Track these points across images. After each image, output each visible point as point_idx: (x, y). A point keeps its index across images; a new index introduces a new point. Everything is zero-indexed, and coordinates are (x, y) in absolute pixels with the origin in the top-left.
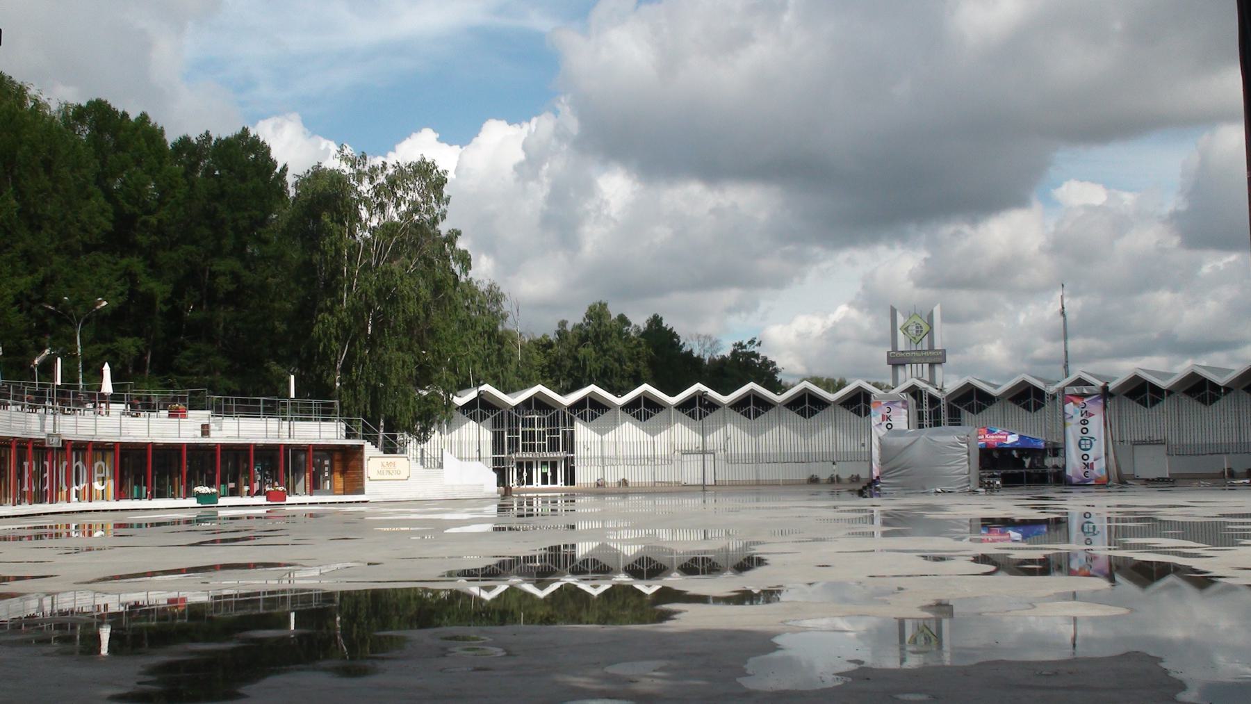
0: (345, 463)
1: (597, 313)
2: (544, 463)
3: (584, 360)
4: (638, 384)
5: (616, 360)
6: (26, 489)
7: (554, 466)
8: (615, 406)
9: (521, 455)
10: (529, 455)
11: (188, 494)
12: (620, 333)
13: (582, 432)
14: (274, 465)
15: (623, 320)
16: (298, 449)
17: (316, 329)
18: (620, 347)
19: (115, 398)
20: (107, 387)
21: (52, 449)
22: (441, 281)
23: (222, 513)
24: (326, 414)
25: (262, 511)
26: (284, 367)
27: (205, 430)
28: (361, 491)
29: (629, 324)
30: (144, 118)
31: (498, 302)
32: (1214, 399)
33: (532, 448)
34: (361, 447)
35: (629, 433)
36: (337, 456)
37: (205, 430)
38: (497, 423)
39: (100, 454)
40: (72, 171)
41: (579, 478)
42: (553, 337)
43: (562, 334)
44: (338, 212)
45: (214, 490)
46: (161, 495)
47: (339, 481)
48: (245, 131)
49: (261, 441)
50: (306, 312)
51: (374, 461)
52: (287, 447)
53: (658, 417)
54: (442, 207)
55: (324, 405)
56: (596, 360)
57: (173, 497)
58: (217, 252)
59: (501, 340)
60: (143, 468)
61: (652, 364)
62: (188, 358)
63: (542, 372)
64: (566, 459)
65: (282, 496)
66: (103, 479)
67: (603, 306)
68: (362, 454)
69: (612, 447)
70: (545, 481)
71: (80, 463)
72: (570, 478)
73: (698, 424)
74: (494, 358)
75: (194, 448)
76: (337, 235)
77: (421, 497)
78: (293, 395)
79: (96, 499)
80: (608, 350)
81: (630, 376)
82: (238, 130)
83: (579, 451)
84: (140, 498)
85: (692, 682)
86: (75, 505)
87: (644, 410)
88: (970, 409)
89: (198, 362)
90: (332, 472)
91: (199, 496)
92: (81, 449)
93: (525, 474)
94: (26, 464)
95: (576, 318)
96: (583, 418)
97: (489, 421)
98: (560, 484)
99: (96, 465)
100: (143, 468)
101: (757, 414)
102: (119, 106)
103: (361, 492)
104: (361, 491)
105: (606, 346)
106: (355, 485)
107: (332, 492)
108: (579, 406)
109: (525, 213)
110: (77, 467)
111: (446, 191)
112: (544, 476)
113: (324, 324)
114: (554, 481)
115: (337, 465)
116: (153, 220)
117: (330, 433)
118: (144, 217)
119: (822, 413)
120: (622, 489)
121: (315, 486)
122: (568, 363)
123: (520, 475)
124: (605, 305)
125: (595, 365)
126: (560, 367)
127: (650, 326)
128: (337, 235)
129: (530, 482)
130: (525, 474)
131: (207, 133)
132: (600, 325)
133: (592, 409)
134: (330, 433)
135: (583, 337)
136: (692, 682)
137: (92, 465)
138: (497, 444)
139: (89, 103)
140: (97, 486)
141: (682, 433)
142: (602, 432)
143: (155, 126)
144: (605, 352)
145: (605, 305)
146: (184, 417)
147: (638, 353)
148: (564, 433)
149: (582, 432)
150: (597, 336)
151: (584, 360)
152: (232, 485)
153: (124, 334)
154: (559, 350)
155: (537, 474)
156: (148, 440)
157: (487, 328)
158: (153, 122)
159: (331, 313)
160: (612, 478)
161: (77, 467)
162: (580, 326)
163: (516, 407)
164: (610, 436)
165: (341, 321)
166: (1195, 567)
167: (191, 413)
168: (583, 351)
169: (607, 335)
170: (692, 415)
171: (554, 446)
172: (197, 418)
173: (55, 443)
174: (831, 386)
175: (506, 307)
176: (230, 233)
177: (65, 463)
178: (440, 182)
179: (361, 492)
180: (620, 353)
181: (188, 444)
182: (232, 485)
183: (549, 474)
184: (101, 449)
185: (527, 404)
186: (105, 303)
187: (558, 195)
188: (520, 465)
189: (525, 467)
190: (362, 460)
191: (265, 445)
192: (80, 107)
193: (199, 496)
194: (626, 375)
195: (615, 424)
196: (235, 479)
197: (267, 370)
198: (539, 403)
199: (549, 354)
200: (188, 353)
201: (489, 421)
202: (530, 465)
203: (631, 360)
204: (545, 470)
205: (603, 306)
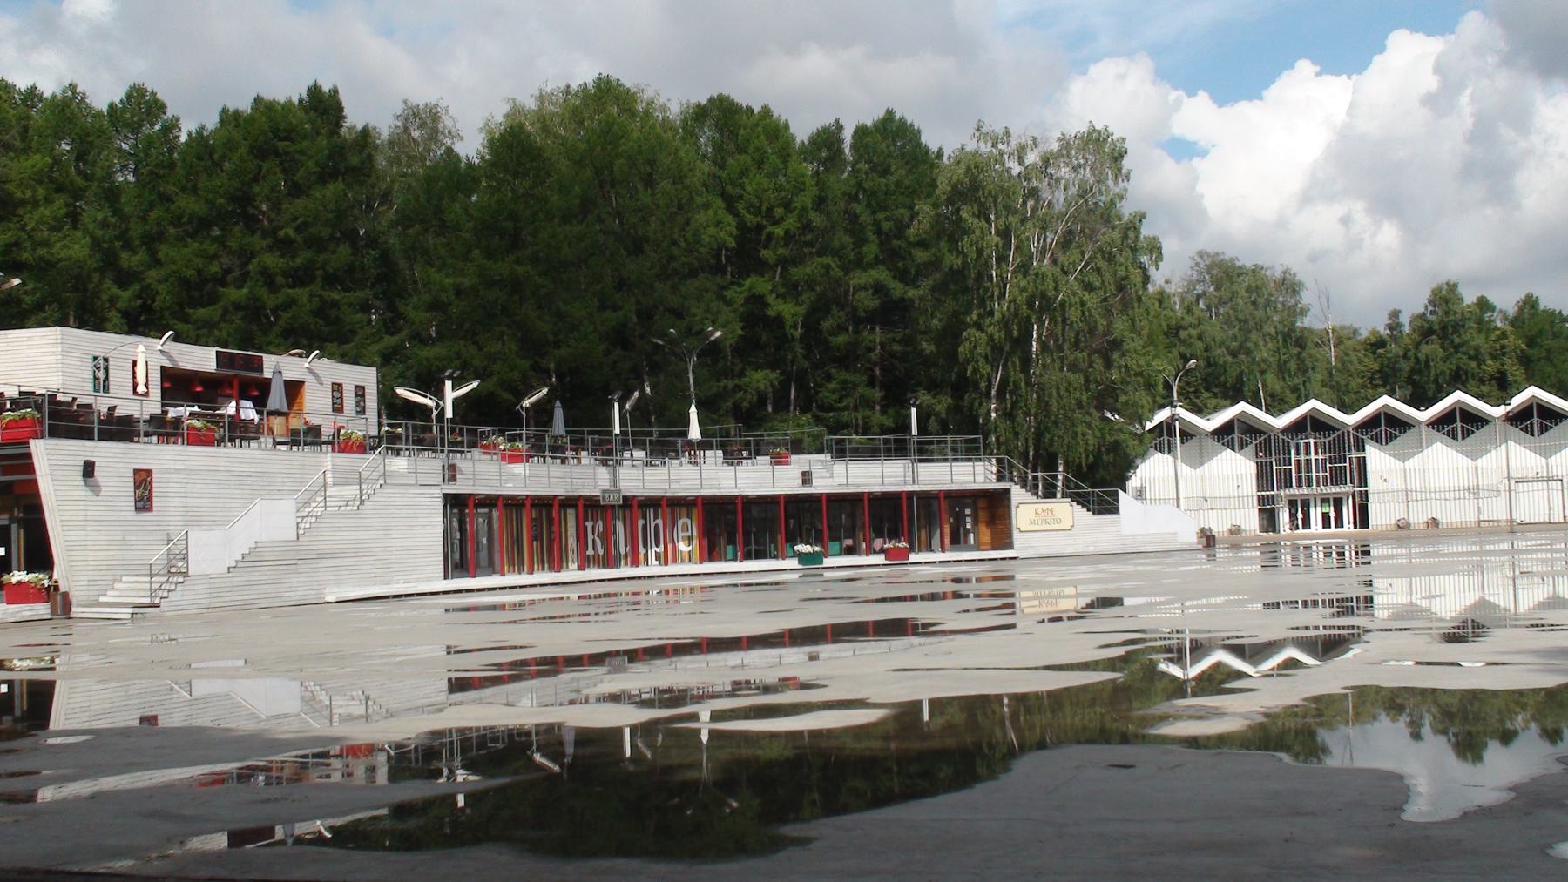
0: (991, 510)
1: (1445, 297)
2: (1325, 501)
3: (1427, 362)
4: (1235, 402)
5: (1471, 358)
6: (590, 552)
7: (1338, 504)
9: (1295, 491)
10: (1304, 490)
11: (871, 551)
12: (1480, 321)
13: (1377, 458)
14: (890, 520)
15: (1483, 304)
16: (927, 500)
17: (961, 349)
18: (1479, 340)
19: (704, 445)
20: (695, 433)
22: (1123, 279)
23: (828, 574)
24: (971, 452)
25: (795, 576)
26: (934, 396)
27: (807, 478)
28: (1009, 545)
29: (1492, 308)
30: (766, 111)
31: (1295, 292)
34: (1007, 491)
35: (1441, 461)
36: (981, 503)
37: (807, 478)
39: (684, 510)
40: (674, 183)
41: (1373, 518)
42: (1384, 332)
43: (1394, 326)
44: (981, 205)
45: (817, 549)
46: (760, 555)
47: (986, 534)
48: (890, 113)
49: (877, 489)
50: (952, 334)
51: (1026, 510)
52: (910, 494)
53: (1481, 434)
54: (1121, 185)
55: (967, 441)
56: (1444, 360)
57: (776, 557)
58: (860, 264)
59: (1301, 343)
60: (734, 526)
61: (1525, 360)
62: (834, 392)
63: (1372, 379)
65: (904, 554)
66: (690, 539)
67: (1453, 287)
68: (1009, 500)
69: (1417, 477)
70: (1326, 524)
71: (660, 522)
72: (1362, 518)
73: (1537, 441)
74: (1293, 365)
75: (793, 501)
76: (978, 232)
77: (1091, 550)
78: (915, 431)
79: (681, 561)
80: (1462, 345)
81: (1492, 378)
82: (881, 114)
83: (1374, 484)
84: (735, 559)
86: (654, 568)
87: (1460, 425)
89: (848, 395)
90: (976, 522)
91: (802, 557)
92: (649, 506)
93: (1300, 515)
94: (589, 524)
95: (1414, 303)
96: (1377, 439)
97: (1251, 449)
98: (1348, 526)
99: (680, 523)
100: (734, 526)
102: (741, 99)
103: (1010, 546)
104: (1009, 545)
105: (1457, 340)
106: (1003, 539)
107: (977, 547)
108: (1371, 424)
109: (1265, 174)
110: (657, 527)
111: (1126, 163)
112: (1326, 517)
113: (974, 342)
114: (1339, 523)
115: (982, 515)
116: (779, 231)
117: (975, 475)
118: (769, 229)
120: (1432, 531)
121: (957, 540)
122: (1405, 366)
123: (1293, 516)
124: (1455, 285)
125: (1442, 367)
126: (1395, 371)
127: (1521, 309)
128: (978, 232)
129: (1306, 524)
130: (1300, 515)
131: (837, 121)
132: (1447, 313)
133: (1388, 428)
134: (975, 475)
135: (1425, 330)
137: (674, 524)
138: (1264, 476)
139: (711, 100)
140: (683, 547)
141: (1519, 455)
142: (1403, 458)
143: (778, 120)
144: (1457, 348)
145: (1455, 285)
146: (787, 463)
147: (1503, 347)
149: (1377, 458)
150: (1444, 328)
151: (1427, 362)
152: (849, 542)
153: (758, 367)
154: (1393, 349)
155: (1316, 514)
156: (735, 492)
157: (1280, 328)
158: (776, 115)
159: (979, 327)
160: (1418, 518)
161: (657, 527)
162: (1422, 316)
163: (1286, 430)
164: (1414, 462)
165: (991, 338)
166: (754, 676)
167: (794, 458)
168: (1425, 349)
169: (1457, 327)
170: (1529, 431)
171: (1337, 477)
172: (799, 462)
173: (614, 499)
175: (1307, 297)
176: (873, 237)
177: (640, 523)
178: (1118, 156)
179: (1010, 546)
180: (1477, 349)
181: (829, 495)
182: (849, 542)
183: (1332, 515)
184: (675, 506)
185: (1298, 427)
186: (718, 334)
187: (1482, 133)
188: (1292, 504)
189: (1300, 507)
190: (1009, 507)
191: (884, 494)
192: (699, 105)
193: (802, 557)
194: (1487, 377)
195: (1420, 448)
196: (852, 535)
198: (1315, 423)
199: (1380, 356)
200: (833, 385)
201: (1251, 449)
202: (1306, 505)
203: (1494, 358)
204: (1326, 510)
205: (1453, 287)
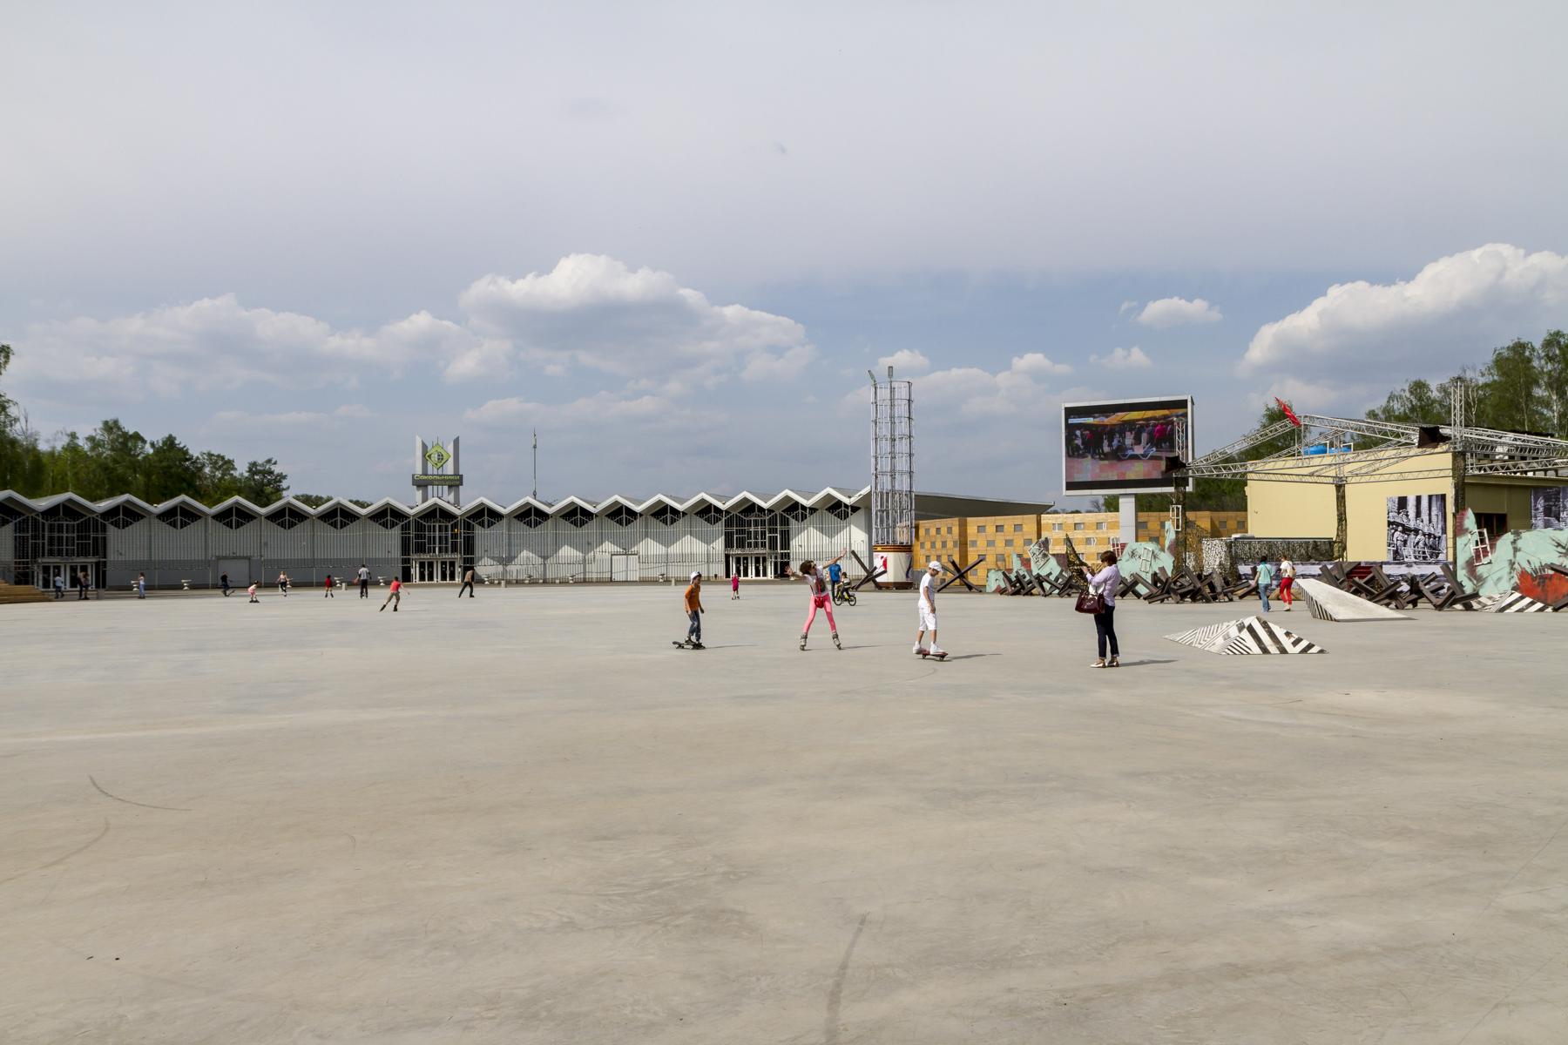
8: (150, 513)
10: (56, 560)
21: (786, 544)
32: (804, 517)
33: (60, 553)
38: (19, 528)
64: (97, 564)
70: (757, 574)
85: (1366, 697)
88: (116, 524)
101: (184, 525)
108: (112, 513)
119: (299, 526)
133: (126, 516)
136: (1366, 697)
148: (96, 539)
171: (83, 552)
174: (317, 501)
185: (52, 512)
197: (1536, 500)
198: (68, 510)
